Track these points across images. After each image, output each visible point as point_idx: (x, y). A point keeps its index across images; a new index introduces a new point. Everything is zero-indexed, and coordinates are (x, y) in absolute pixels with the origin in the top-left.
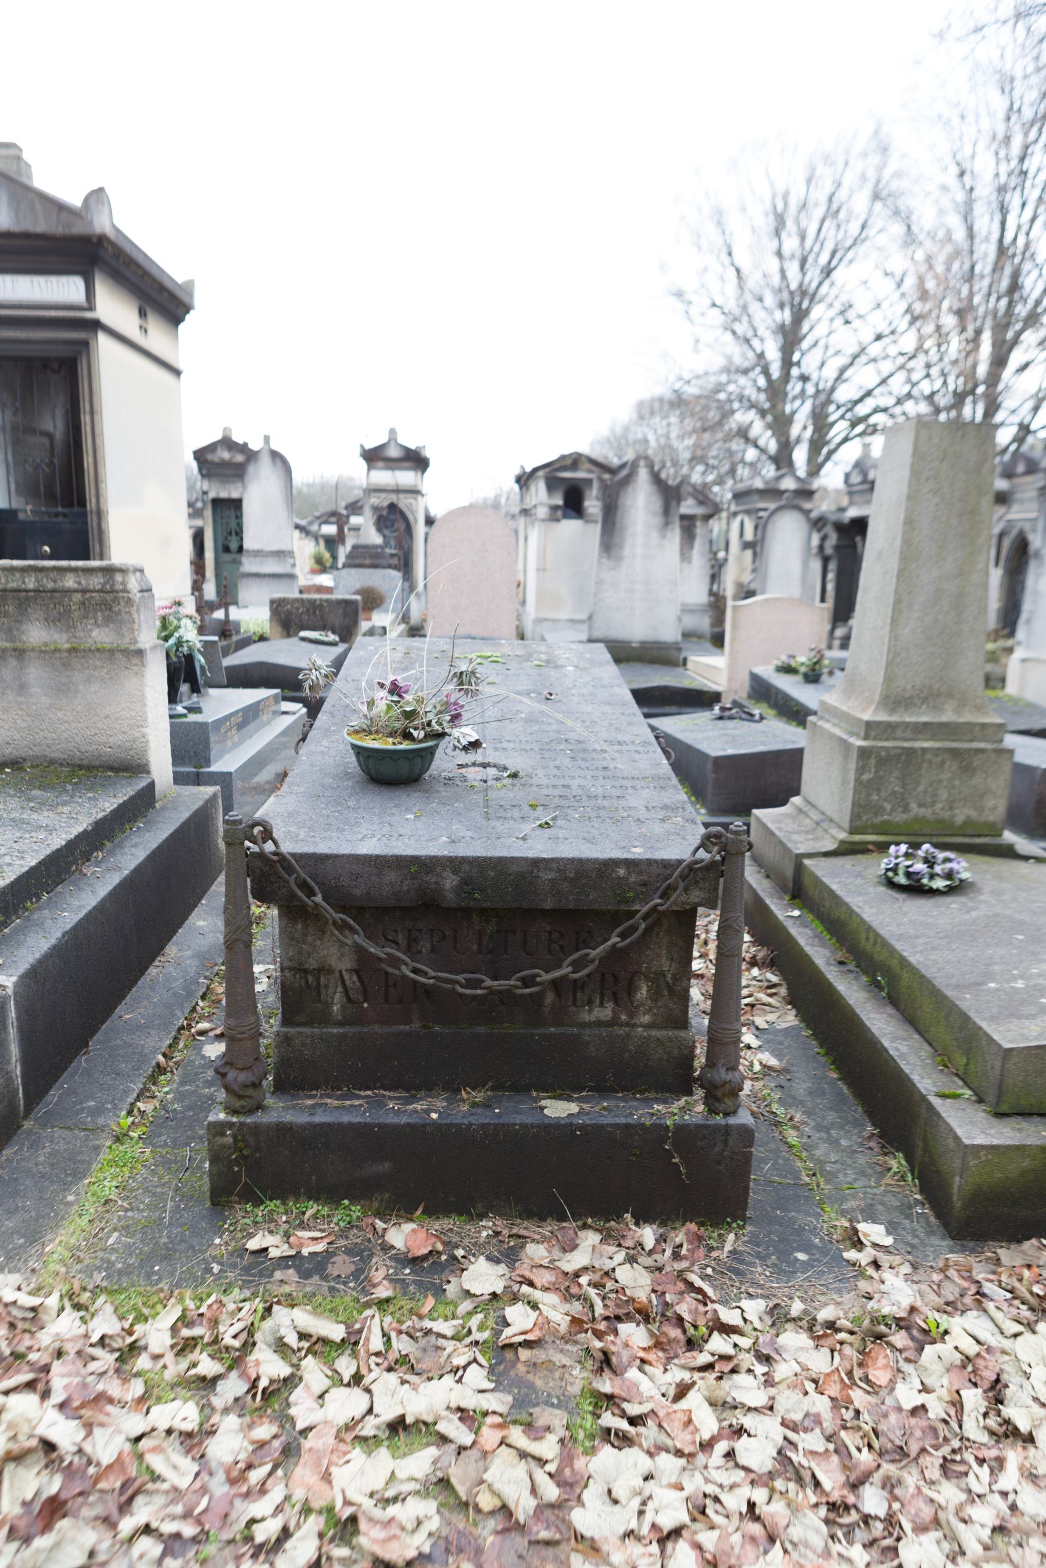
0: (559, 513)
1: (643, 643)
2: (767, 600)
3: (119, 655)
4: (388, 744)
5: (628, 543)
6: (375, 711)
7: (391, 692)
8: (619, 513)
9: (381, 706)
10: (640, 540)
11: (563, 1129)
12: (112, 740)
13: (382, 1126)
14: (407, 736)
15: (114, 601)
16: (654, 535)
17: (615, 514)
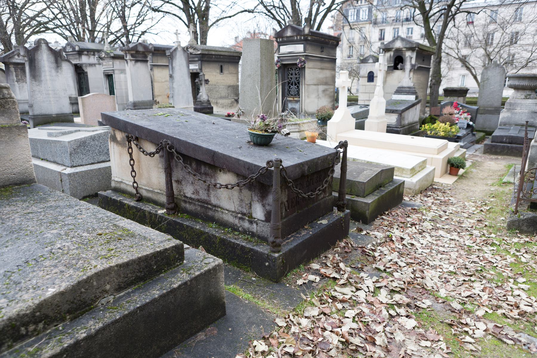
0: (392, 68)
1: (56, 114)
2: (93, 95)
3: (14, 129)
4: (260, 133)
5: (43, 74)
6: (256, 124)
7: (262, 119)
8: (36, 62)
9: (258, 123)
10: (47, 73)
11: (329, 226)
12: (15, 171)
13: (306, 239)
14: (266, 131)
15: (5, 103)
16: (53, 71)
17: (35, 63)
